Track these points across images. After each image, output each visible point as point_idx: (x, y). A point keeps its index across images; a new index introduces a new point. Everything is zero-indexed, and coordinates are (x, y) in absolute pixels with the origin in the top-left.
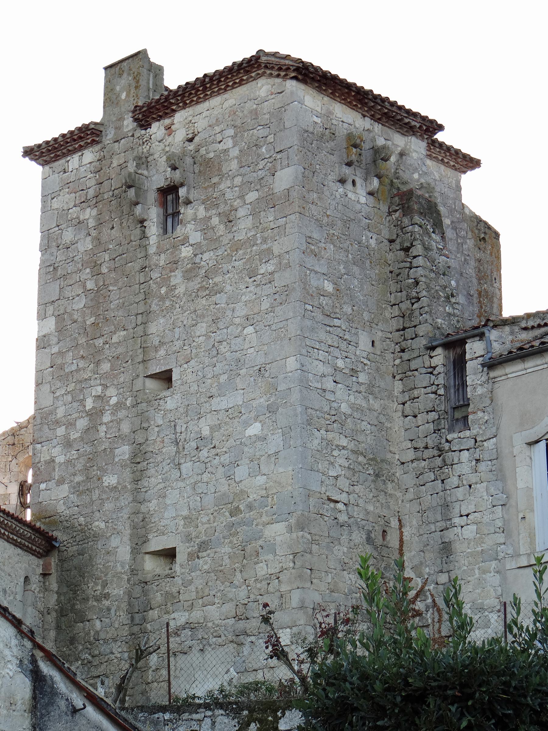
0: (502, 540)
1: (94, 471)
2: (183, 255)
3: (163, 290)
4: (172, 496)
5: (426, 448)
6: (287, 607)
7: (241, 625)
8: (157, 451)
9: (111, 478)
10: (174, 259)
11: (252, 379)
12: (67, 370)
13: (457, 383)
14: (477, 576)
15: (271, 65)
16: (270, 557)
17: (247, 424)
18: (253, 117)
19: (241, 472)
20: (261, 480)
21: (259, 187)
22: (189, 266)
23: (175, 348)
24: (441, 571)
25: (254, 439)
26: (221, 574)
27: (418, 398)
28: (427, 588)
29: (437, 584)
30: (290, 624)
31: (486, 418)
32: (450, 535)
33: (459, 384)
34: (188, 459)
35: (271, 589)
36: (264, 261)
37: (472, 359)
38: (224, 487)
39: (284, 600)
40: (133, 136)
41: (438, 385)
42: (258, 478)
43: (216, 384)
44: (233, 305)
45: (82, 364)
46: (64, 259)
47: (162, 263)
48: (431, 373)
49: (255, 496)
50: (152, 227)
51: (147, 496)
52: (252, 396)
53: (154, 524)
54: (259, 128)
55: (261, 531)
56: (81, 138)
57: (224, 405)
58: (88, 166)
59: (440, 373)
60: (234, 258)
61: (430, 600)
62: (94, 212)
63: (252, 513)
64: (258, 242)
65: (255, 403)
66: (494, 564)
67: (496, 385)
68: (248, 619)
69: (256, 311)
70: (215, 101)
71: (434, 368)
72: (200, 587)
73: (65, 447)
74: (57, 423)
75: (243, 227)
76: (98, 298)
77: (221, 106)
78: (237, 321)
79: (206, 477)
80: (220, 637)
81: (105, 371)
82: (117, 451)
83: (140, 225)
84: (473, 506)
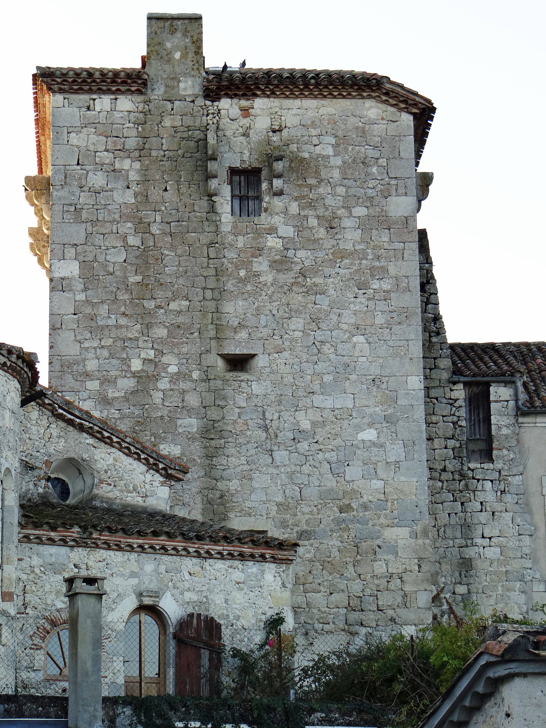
0: (530, 566)
1: (146, 435)
2: (269, 244)
3: (242, 273)
4: (261, 481)
5: (444, 470)
6: (412, 605)
7: (356, 616)
8: (238, 433)
9: (173, 448)
10: (258, 246)
11: (365, 387)
12: (100, 323)
13: (473, 418)
14: (500, 592)
15: (394, 94)
16: (391, 557)
17: (359, 428)
18: (359, 135)
19: (353, 472)
20: (378, 484)
21: (369, 205)
22: (278, 257)
23: (260, 335)
24: (460, 583)
25: (368, 444)
26: (329, 566)
27: (436, 424)
28: (442, 595)
29: (454, 593)
30: (416, 622)
31: (512, 456)
32: (471, 552)
33: (475, 420)
34: (282, 447)
35: (392, 586)
36: (377, 277)
37: (496, 402)
38: (330, 482)
39: (409, 599)
40: (193, 101)
41: (459, 417)
42: (374, 481)
43: (319, 382)
44: (338, 310)
45: (123, 321)
46: (92, 203)
47: (240, 245)
48: (451, 404)
49: (370, 497)
50: (225, 205)
51: (226, 474)
52: (366, 403)
53: (237, 504)
54: (367, 147)
55: (379, 531)
56: (124, 82)
57: (329, 404)
58: (126, 113)
59: (461, 406)
60: (338, 265)
61: (445, 607)
62: (137, 165)
63: (367, 513)
64: (370, 257)
65: (368, 411)
66: (518, 585)
67: (522, 430)
68: (363, 611)
69: (369, 322)
70: (310, 103)
71: (456, 400)
72: (301, 574)
73: (100, 403)
74: (87, 375)
75: (350, 238)
76: (145, 259)
77: (317, 110)
78: (345, 327)
79: (306, 469)
80: (329, 623)
81: (160, 336)
82: (179, 422)
83: (206, 198)
84: (498, 532)
